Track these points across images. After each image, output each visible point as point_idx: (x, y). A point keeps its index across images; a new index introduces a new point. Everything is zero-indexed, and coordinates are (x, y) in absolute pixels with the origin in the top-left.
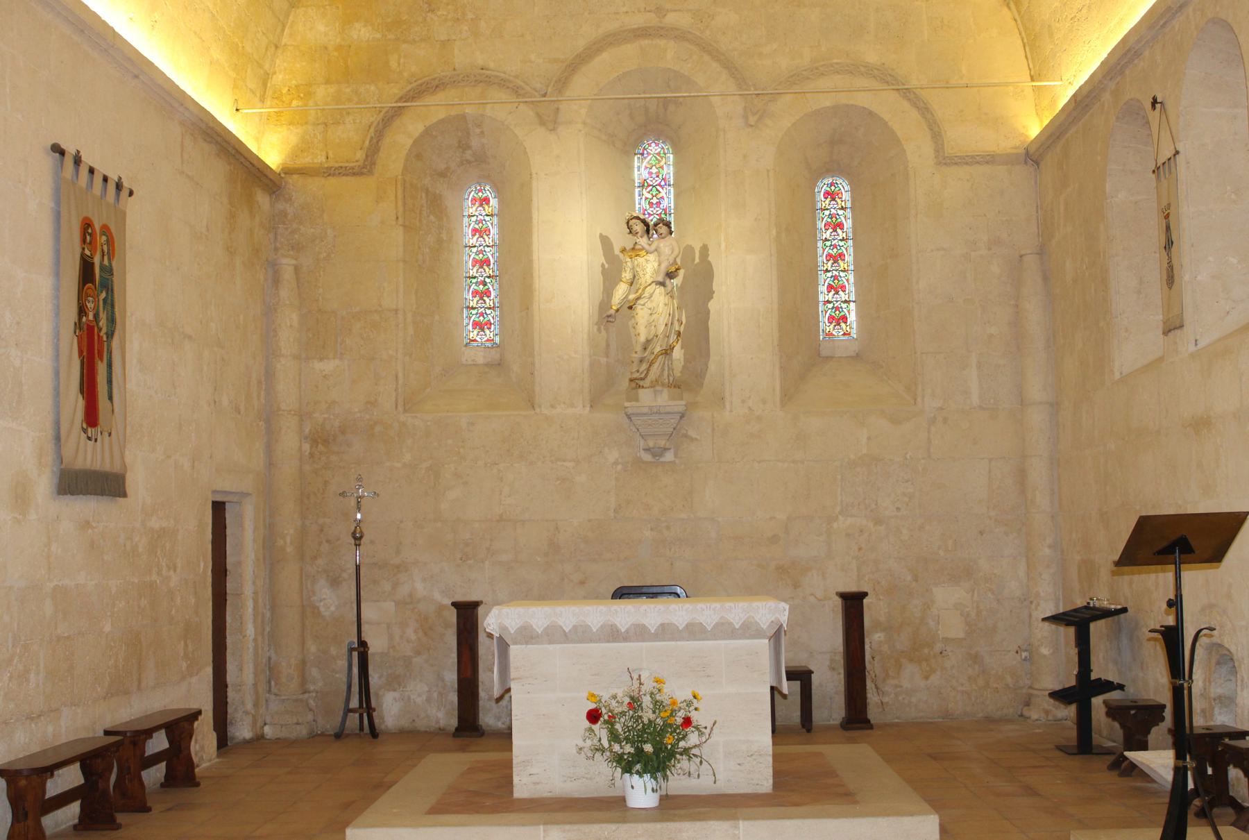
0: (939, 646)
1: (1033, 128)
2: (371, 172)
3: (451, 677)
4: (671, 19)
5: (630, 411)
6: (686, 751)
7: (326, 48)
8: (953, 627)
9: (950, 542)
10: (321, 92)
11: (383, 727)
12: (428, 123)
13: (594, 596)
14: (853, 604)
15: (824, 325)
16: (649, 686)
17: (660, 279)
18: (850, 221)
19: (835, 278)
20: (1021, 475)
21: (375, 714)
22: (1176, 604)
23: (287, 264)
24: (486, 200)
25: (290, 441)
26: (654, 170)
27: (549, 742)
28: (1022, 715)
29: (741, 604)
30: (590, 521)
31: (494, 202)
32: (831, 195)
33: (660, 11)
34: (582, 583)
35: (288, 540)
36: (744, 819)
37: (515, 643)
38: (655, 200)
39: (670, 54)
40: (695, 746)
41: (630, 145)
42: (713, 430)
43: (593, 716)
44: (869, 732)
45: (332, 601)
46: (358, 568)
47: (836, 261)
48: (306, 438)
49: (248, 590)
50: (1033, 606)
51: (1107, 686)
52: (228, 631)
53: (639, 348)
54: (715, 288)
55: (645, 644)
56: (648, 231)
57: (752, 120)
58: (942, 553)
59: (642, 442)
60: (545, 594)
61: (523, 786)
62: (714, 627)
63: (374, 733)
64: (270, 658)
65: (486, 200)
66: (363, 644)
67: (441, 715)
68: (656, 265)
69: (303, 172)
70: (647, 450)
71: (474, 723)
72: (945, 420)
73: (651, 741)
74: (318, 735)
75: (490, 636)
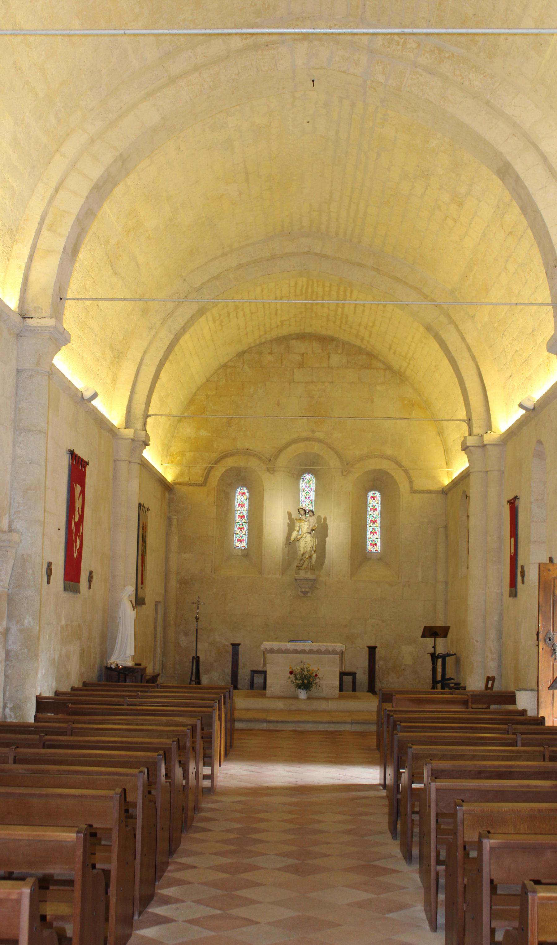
0: (403, 667)
1: (446, 481)
2: (205, 485)
4: (317, 434)
5: (297, 578)
7: (190, 438)
8: (408, 660)
10: (189, 455)
12: (227, 468)
14: (372, 650)
15: (369, 547)
17: (309, 531)
18: (380, 508)
19: (373, 529)
22: (434, 647)
23: (174, 518)
24: (244, 493)
25: (173, 583)
26: (308, 485)
31: (247, 494)
32: (373, 498)
33: (313, 431)
38: (307, 497)
39: (316, 448)
41: (298, 476)
43: (291, 673)
45: (184, 641)
47: (374, 523)
53: (300, 556)
54: (329, 533)
56: (305, 513)
57: (345, 474)
61: (267, 695)
65: (244, 493)
66: (198, 657)
68: (308, 526)
69: (180, 484)
70: (302, 592)
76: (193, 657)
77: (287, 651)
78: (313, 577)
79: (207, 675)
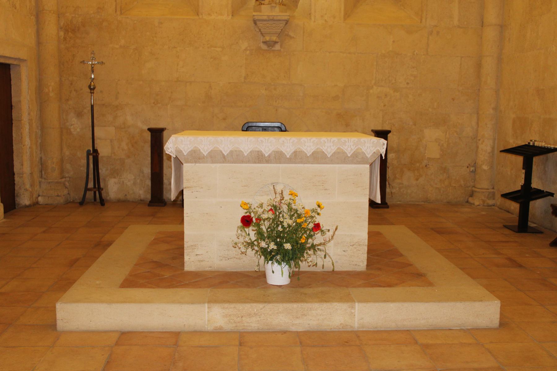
0: (425, 162)
3: (147, 170)
5: (256, 18)
6: (313, 247)
8: (433, 152)
9: (436, 104)
11: (108, 198)
13: (229, 127)
16: (287, 197)
20: (479, 66)
21: (102, 192)
25: (51, 29)
27: (211, 233)
28: (467, 202)
29: (353, 139)
30: (229, 83)
34: (224, 119)
35: (51, 89)
36: (360, 301)
37: (187, 162)
40: (320, 244)
42: (304, 32)
43: (246, 221)
44: (386, 210)
46: (92, 107)
48: (61, 28)
49: (25, 118)
50: (480, 142)
51: (540, 194)
52: (14, 142)
55: (281, 165)
58: (430, 110)
59: (262, 38)
60: (203, 126)
61: (191, 262)
62: (332, 155)
63: (102, 202)
64: (41, 158)
66: (95, 151)
67: (141, 192)
70: (264, 42)
71: (162, 201)
72: (438, 33)
73: (285, 237)
74: (70, 202)
75: (169, 157)
76: (88, 151)
77: (236, 157)
78: (285, 16)
79: (115, 178)
